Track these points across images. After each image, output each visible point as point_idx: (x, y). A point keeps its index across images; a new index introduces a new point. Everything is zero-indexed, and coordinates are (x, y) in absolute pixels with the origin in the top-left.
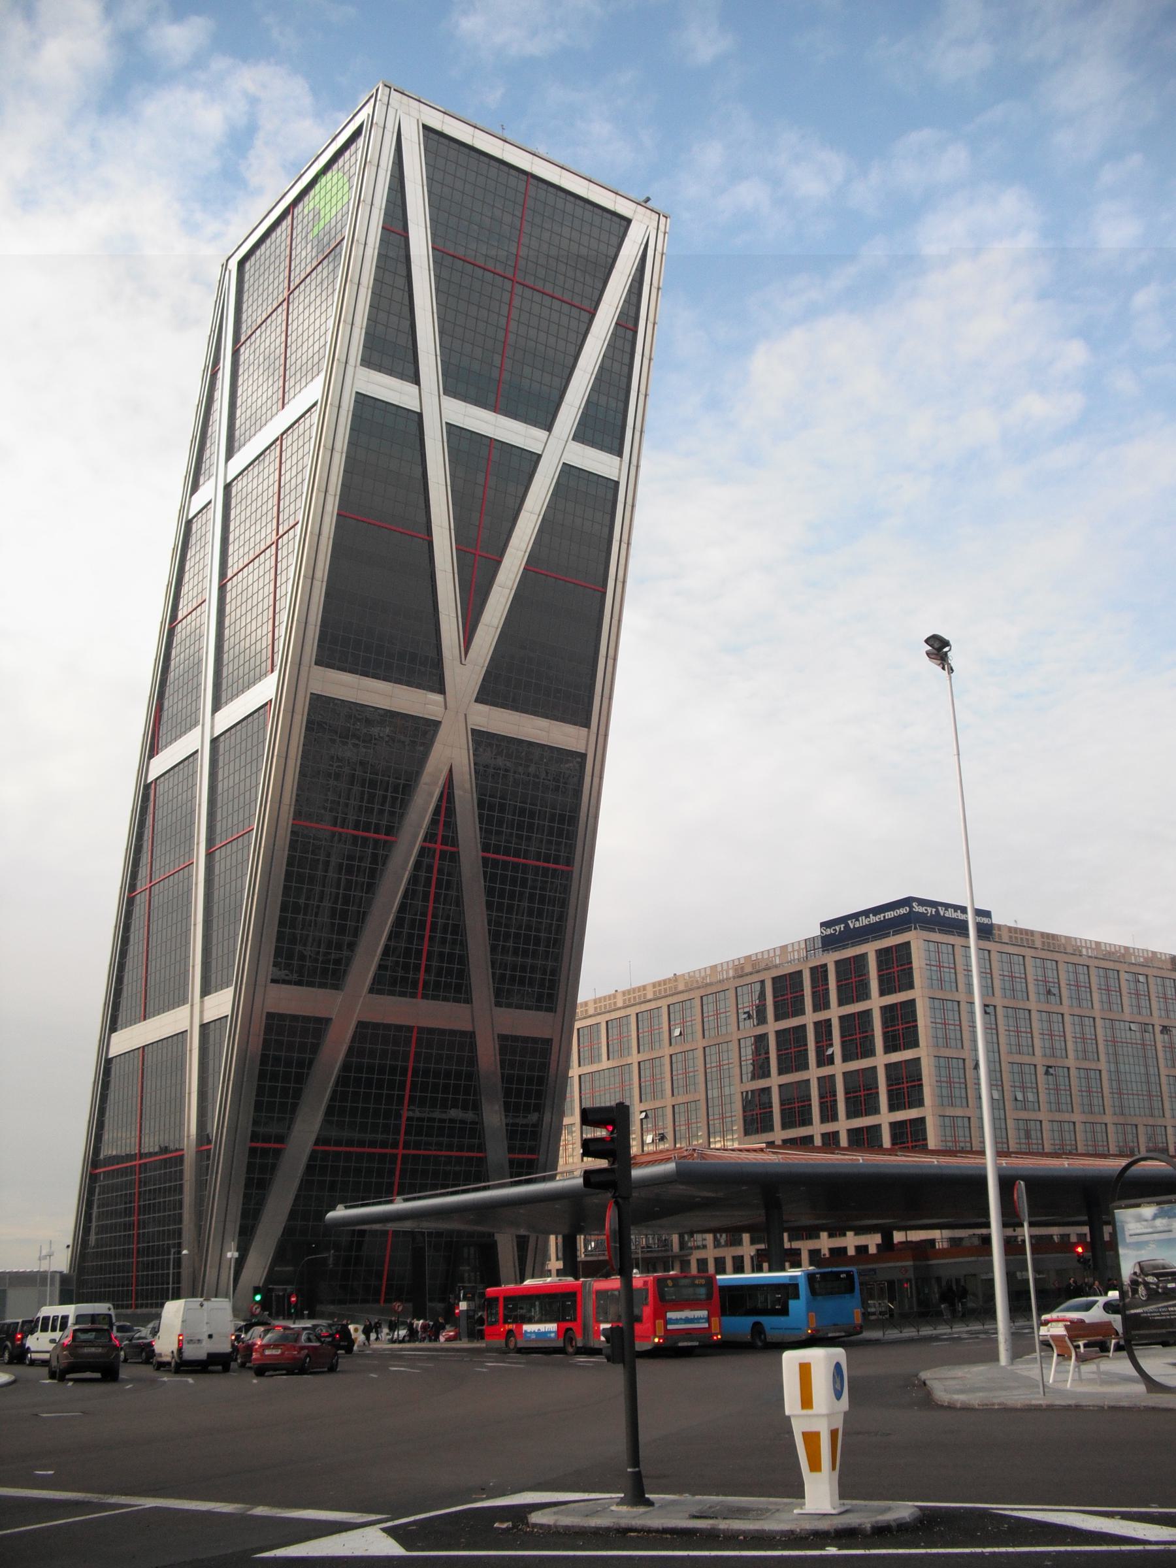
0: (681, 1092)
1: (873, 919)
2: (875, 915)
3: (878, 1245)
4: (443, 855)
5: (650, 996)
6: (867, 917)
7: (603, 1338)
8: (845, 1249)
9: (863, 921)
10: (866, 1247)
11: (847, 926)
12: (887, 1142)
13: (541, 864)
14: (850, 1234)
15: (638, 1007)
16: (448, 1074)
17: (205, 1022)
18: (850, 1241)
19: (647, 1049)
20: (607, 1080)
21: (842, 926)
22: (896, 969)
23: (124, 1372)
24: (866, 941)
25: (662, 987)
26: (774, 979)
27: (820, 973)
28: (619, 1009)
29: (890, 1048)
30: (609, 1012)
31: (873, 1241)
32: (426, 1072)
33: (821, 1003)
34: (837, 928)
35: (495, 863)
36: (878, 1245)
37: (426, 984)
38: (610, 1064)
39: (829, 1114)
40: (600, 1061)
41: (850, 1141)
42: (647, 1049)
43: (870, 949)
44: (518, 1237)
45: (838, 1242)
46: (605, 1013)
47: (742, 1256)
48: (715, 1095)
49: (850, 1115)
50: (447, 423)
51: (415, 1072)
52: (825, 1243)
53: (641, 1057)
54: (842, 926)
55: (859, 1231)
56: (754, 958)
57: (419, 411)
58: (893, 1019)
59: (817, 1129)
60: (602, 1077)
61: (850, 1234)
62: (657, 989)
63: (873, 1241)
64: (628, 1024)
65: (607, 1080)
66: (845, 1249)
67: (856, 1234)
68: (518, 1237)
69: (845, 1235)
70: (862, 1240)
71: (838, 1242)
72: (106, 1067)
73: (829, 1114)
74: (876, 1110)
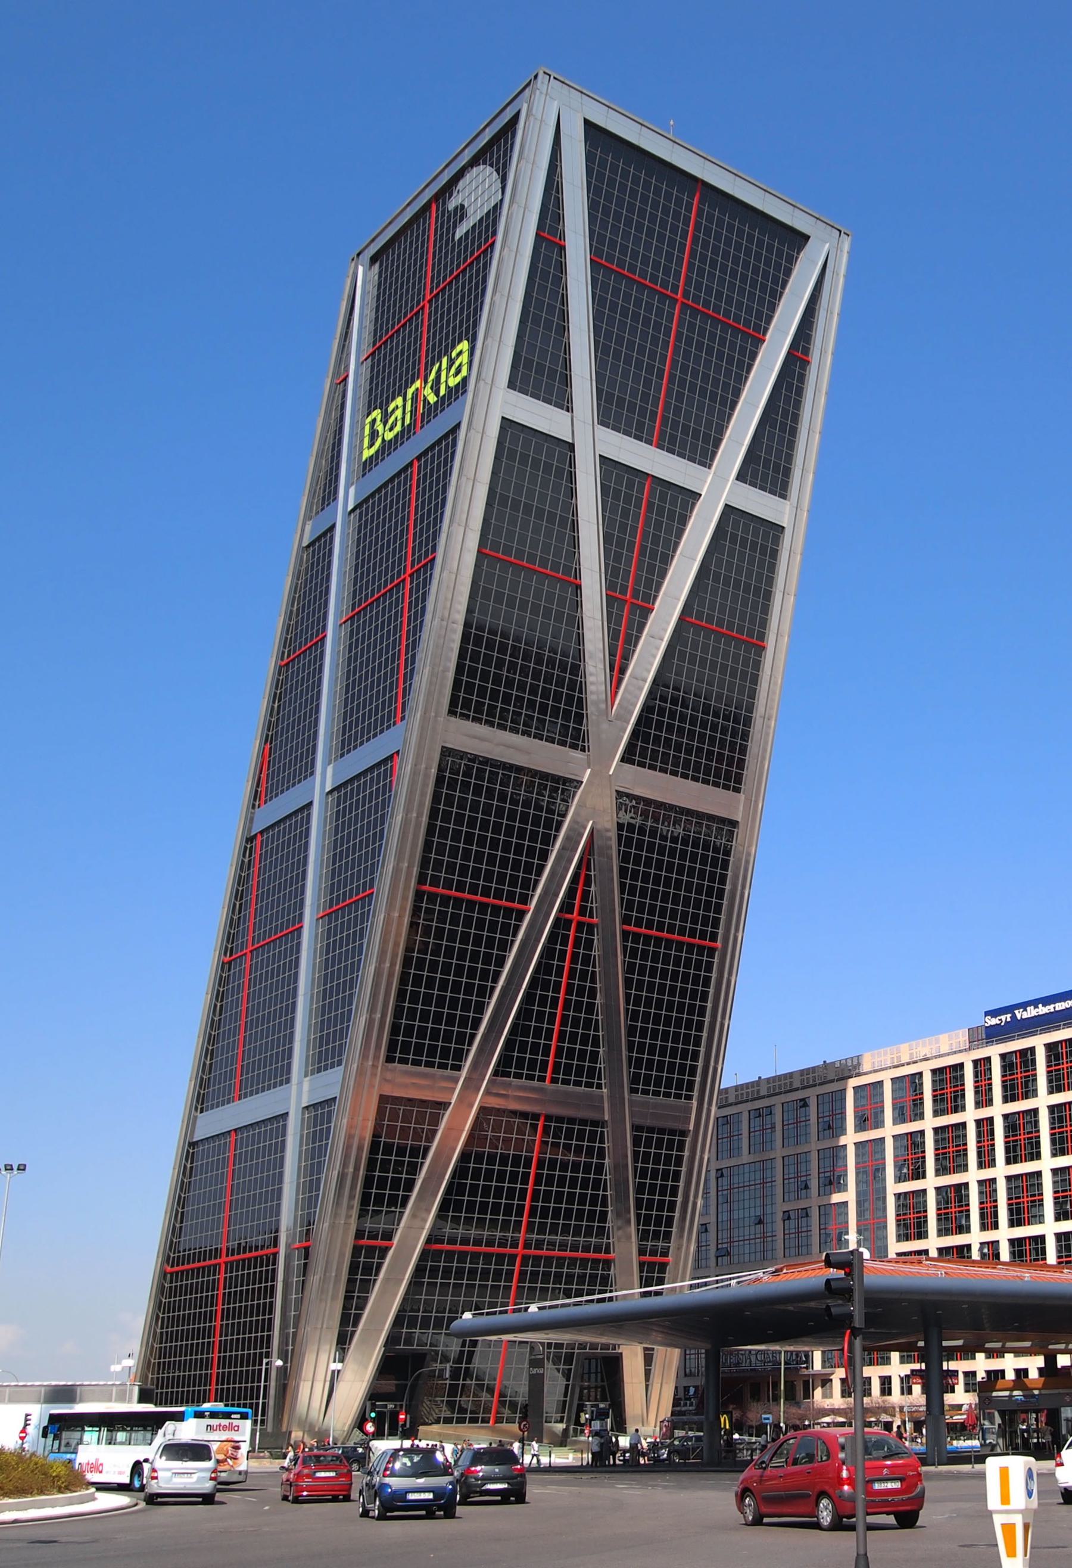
0: (792, 1198)
1: (1043, 1010)
2: (1044, 1005)
3: (1040, 1370)
4: (580, 926)
5: (764, 1092)
6: (1036, 1007)
7: (382, 1446)
8: (1003, 1372)
9: (1031, 1012)
10: (1026, 1371)
11: (1014, 1016)
12: (1052, 1257)
13: (686, 939)
14: (980, 1356)
15: (749, 1104)
16: (564, 1166)
17: (195, 1140)
18: (1009, 1364)
19: (725, 1155)
20: (747, 1175)
21: (1009, 1016)
22: (1019, 1075)
23: (460, 1510)
24: (1034, 1034)
25: (811, 1076)
26: (934, 1072)
27: (982, 1066)
28: (763, 1097)
29: (940, 1171)
30: (786, 1092)
31: (1034, 1364)
32: (553, 1164)
33: (984, 1099)
34: (1003, 1018)
35: (636, 937)
36: (1040, 1370)
37: (556, 1067)
38: (752, 1158)
39: (989, 1221)
40: (739, 1155)
41: (1013, 1254)
42: (725, 1155)
43: (1039, 1042)
44: (646, 1349)
45: (995, 1364)
46: (747, 1101)
47: (890, 1377)
48: (725, 1219)
49: (1013, 1223)
50: (600, 456)
51: (540, 1164)
52: (981, 1365)
53: (786, 1152)
54: (1009, 1016)
55: (1018, 1352)
56: (837, 1065)
57: (570, 441)
58: (1061, 1119)
59: (975, 1237)
60: (741, 1172)
61: (980, 1356)
62: (739, 1093)
63: (1034, 1364)
64: (739, 1122)
65: (747, 1175)
66: (1003, 1372)
67: (1015, 1356)
68: (646, 1349)
69: (974, 1358)
70: (1023, 1362)
71: (995, 1364)
72: (192, 1150)
73: (989, 1221)
74: (1040, 1219)
